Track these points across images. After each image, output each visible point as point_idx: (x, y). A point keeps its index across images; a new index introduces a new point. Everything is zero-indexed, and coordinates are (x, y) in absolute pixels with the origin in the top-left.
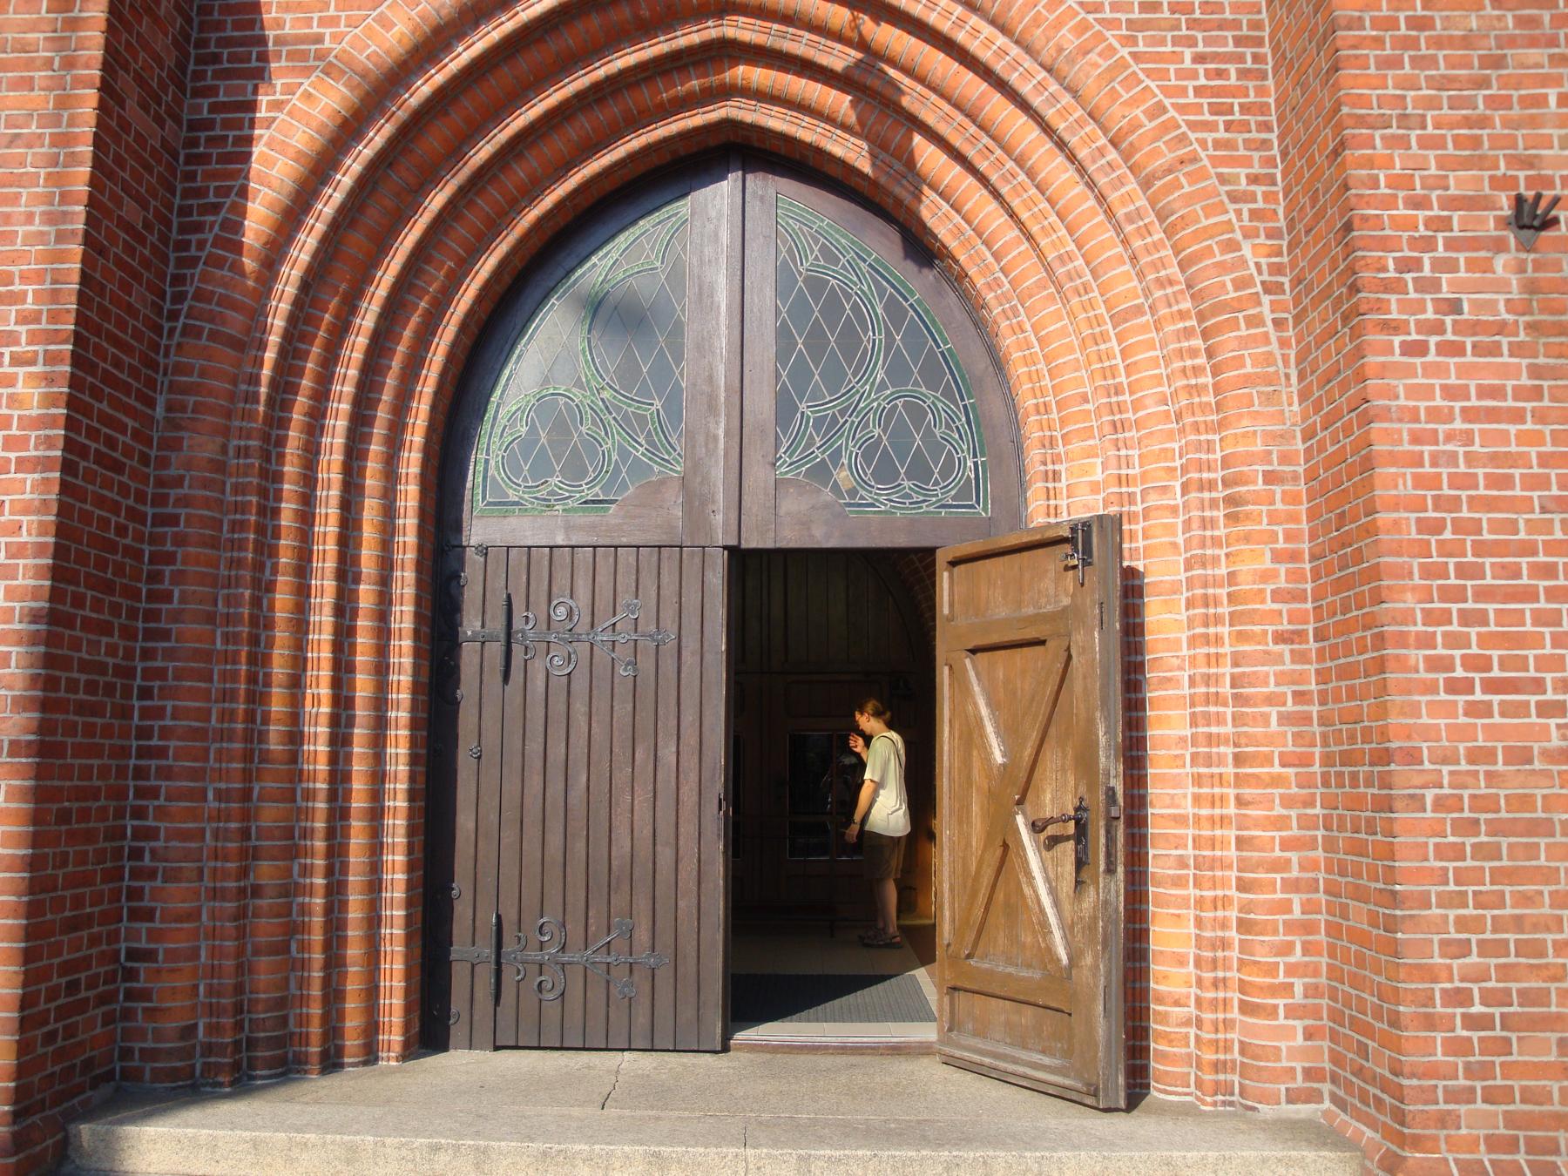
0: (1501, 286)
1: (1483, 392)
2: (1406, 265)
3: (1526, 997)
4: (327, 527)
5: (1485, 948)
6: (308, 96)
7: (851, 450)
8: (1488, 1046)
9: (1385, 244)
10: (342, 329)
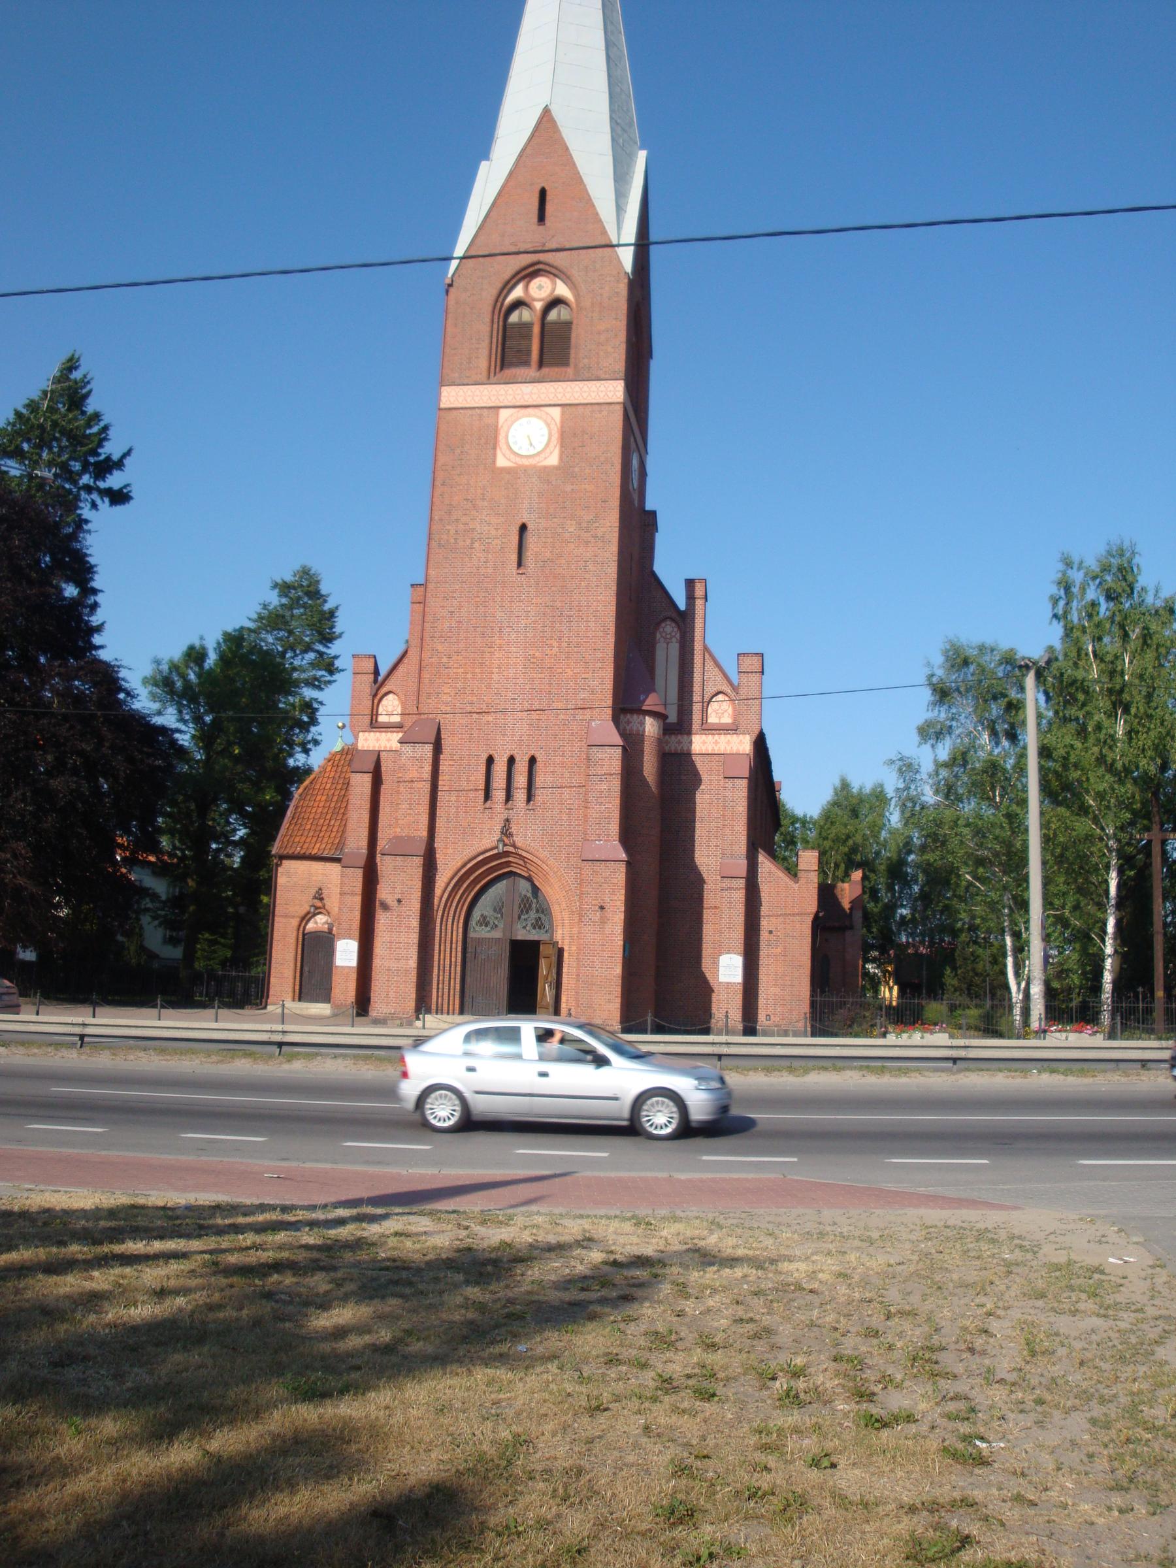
4: (449, 936)
7: (529, 925)
10: (468, 896)
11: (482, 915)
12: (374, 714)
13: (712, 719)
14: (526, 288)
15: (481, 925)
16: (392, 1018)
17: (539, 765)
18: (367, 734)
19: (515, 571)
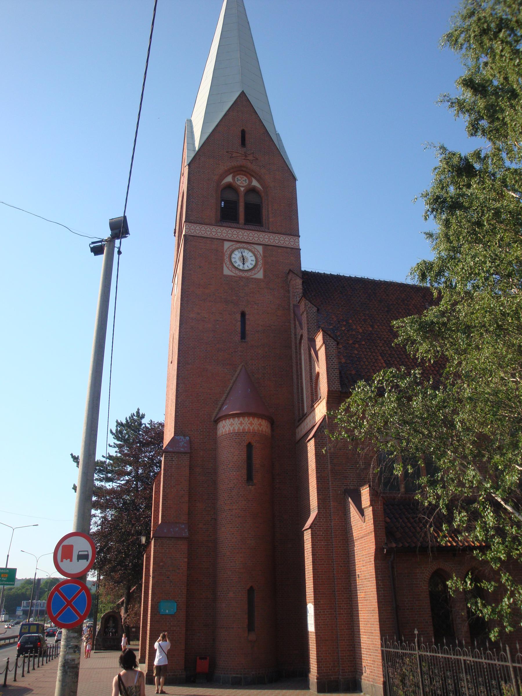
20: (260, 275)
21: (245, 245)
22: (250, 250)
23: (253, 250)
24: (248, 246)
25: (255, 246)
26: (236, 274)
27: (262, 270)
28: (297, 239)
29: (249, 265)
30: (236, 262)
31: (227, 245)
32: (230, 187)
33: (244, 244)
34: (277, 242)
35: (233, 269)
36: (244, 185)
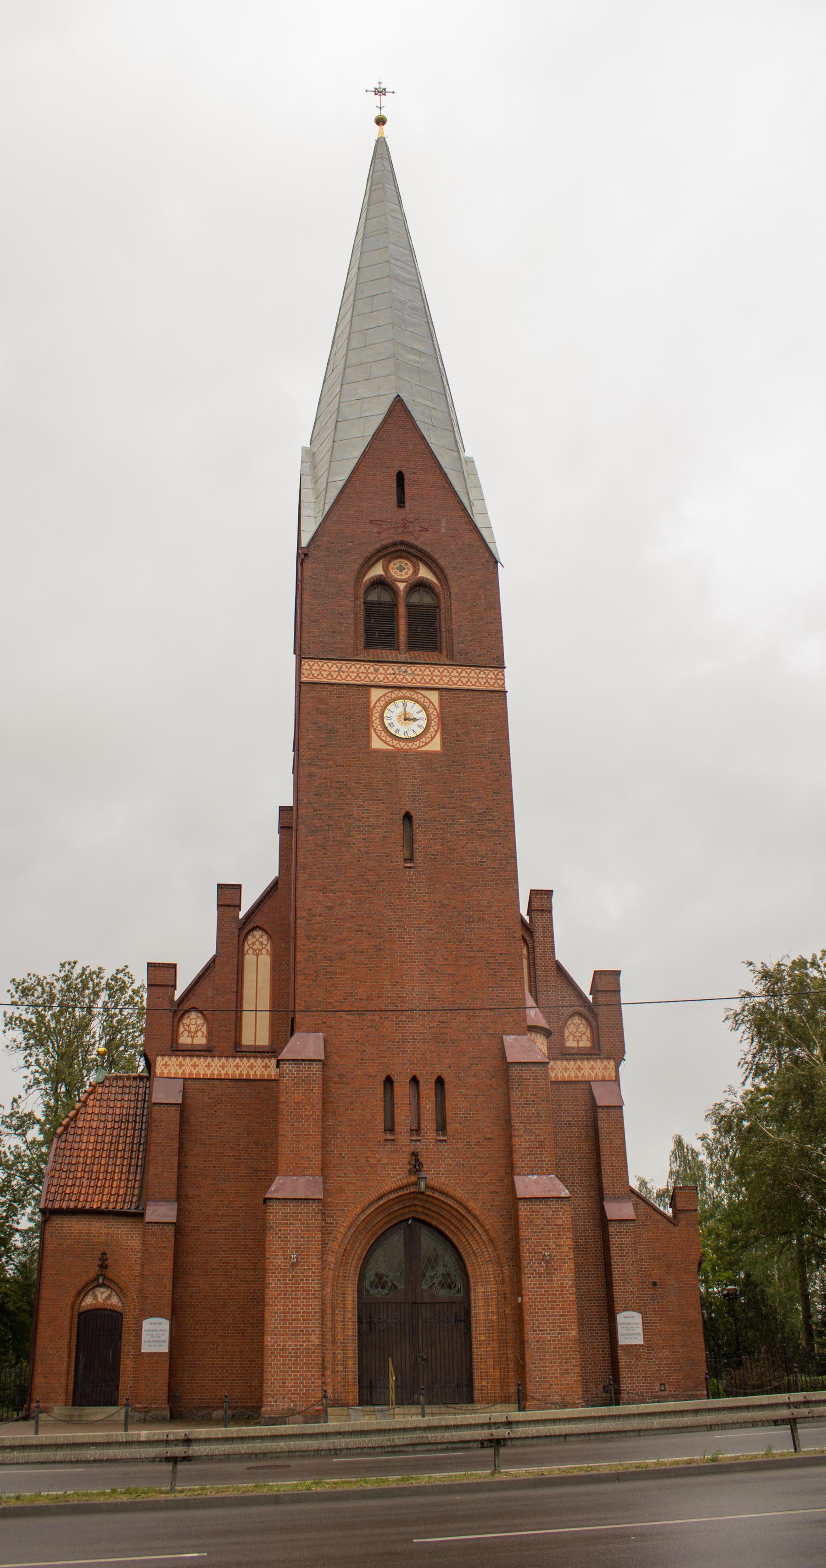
0: (542, 1266)
1: (539, 1284)
2: (528, 1264)
3: (544, 1378)
5: (539, 1370)
6: (343, 1222)
8: (539, 1385)
9: (526, 1260)
11: (377, 1274)
12: (175, 1034)
13: (185, 1039)
14: (386, 569)
15: (376, 1287)
16: (293, 1414)
17: (448, 1087)
18: (166, 1059)
19: (401, 864)
20: (435, 745)
21: (407, 693)
22: (416, 701)
23: (422, 700)
24: (412, 693)
25: (423, 692)
26: (393, 746)
27: (439, 734)
28: (500, 674)
29: (415, 729)
30: (391, 725)
31: (375, 694)
32: (380, 583)
33: (404, 691)
34: (381, 679)
35: (389, 739)
36: (404, 577)
